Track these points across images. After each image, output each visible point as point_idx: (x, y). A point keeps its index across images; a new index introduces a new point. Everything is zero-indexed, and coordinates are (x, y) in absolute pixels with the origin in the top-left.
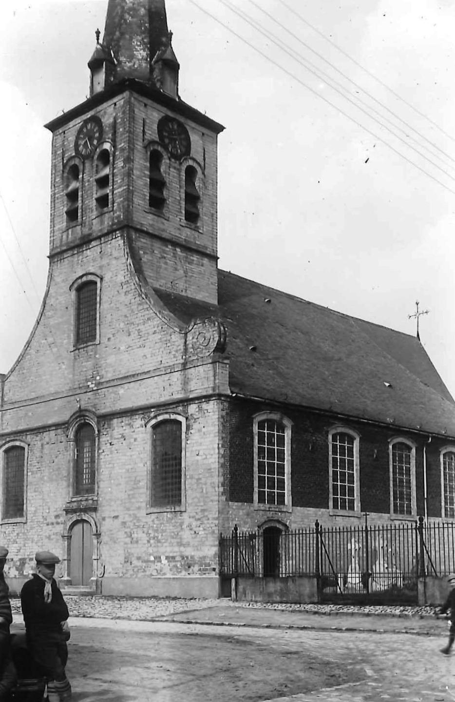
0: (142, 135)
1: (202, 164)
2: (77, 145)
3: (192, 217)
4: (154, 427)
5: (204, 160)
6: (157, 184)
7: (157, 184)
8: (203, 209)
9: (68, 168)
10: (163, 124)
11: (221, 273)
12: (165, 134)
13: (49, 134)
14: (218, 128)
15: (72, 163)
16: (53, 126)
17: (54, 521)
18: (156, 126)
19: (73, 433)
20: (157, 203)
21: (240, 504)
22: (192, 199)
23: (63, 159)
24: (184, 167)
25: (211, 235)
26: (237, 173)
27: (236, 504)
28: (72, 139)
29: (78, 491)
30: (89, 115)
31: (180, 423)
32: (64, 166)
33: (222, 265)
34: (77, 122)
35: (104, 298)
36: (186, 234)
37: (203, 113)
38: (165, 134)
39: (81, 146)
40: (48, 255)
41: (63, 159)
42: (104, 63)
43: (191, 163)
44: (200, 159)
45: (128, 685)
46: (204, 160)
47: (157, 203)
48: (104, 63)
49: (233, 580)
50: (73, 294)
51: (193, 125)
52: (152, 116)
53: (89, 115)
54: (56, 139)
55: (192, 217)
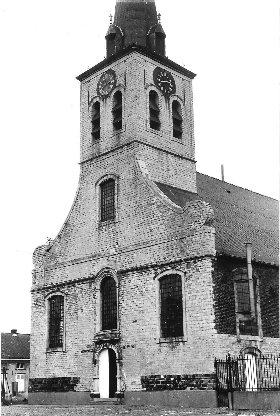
0: (144, 80)
1: (183, 99)
2: (98, 90)
3: (178, 134)
4: (50, 300)
5: (184, 96)
6: (154, 113)
7: (154, 113)
8: (184, 126)
9: (92, 104)
10: (157, 72)
11: (198, 174)
12: (158, 80)
13: (79, 82)
14: (192, 75)
15: (95, 101)
16: (82, 78)
17: (87, 349)
18: (152, 74)
19: (101, 279)
20: (155, 125)
21: (228, 335)
22: (177, 122)
23: (88, 98)
24: (171, 101)
25: (191, 147)
26: (204, 103)
27: (225, 335)
28: (95, 86)
29: (104, 327)
30: (106, 69)
31: (180, 276)
32: (89, 104)
33: (201, 168)
34: (99, 73)
35: (121, 191)
36: (175, 146)
37: (182, 65)
38: (158, 80)
39: (103, 90)
40: (79, 162)
41: (88, 98)
42: (20, 364)
43: (176, 98)
44: (182, 96)
45: (168, 342)
46: (184, 96)
47: (155, 125)
48: (20, 364)
49: (230, 394)
50: (98, 189)
51: (177, 73)
52: (150, 66)
53: (106, 69)
54: (83, 86)
55: (178, 134)
